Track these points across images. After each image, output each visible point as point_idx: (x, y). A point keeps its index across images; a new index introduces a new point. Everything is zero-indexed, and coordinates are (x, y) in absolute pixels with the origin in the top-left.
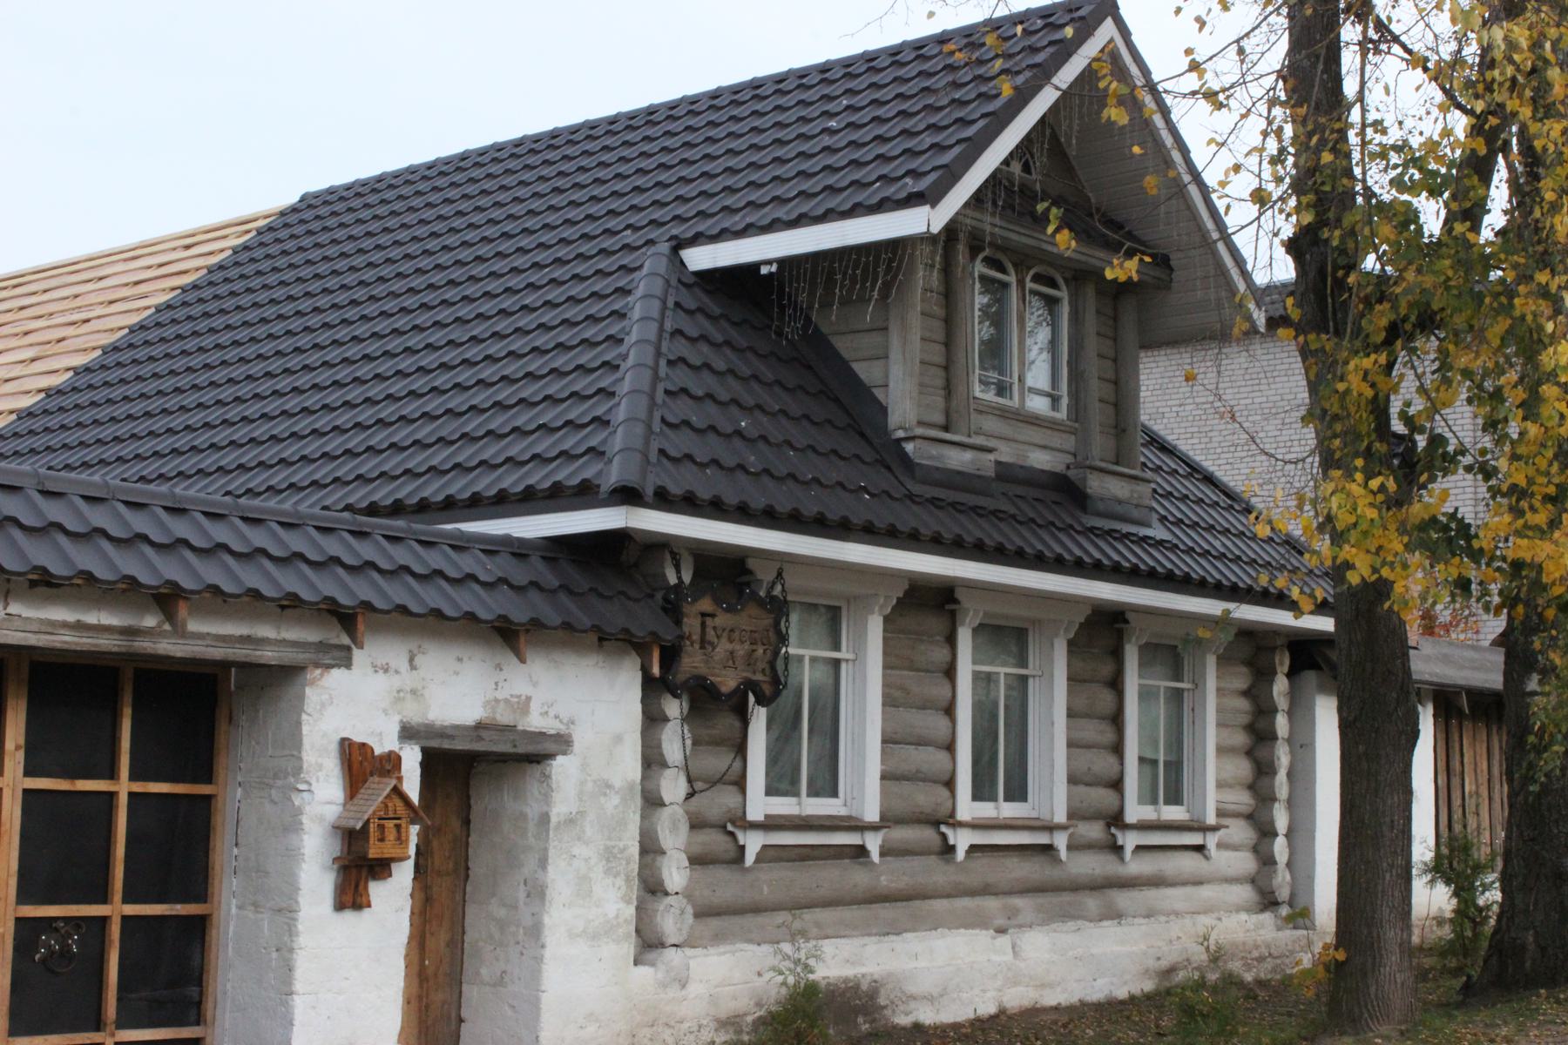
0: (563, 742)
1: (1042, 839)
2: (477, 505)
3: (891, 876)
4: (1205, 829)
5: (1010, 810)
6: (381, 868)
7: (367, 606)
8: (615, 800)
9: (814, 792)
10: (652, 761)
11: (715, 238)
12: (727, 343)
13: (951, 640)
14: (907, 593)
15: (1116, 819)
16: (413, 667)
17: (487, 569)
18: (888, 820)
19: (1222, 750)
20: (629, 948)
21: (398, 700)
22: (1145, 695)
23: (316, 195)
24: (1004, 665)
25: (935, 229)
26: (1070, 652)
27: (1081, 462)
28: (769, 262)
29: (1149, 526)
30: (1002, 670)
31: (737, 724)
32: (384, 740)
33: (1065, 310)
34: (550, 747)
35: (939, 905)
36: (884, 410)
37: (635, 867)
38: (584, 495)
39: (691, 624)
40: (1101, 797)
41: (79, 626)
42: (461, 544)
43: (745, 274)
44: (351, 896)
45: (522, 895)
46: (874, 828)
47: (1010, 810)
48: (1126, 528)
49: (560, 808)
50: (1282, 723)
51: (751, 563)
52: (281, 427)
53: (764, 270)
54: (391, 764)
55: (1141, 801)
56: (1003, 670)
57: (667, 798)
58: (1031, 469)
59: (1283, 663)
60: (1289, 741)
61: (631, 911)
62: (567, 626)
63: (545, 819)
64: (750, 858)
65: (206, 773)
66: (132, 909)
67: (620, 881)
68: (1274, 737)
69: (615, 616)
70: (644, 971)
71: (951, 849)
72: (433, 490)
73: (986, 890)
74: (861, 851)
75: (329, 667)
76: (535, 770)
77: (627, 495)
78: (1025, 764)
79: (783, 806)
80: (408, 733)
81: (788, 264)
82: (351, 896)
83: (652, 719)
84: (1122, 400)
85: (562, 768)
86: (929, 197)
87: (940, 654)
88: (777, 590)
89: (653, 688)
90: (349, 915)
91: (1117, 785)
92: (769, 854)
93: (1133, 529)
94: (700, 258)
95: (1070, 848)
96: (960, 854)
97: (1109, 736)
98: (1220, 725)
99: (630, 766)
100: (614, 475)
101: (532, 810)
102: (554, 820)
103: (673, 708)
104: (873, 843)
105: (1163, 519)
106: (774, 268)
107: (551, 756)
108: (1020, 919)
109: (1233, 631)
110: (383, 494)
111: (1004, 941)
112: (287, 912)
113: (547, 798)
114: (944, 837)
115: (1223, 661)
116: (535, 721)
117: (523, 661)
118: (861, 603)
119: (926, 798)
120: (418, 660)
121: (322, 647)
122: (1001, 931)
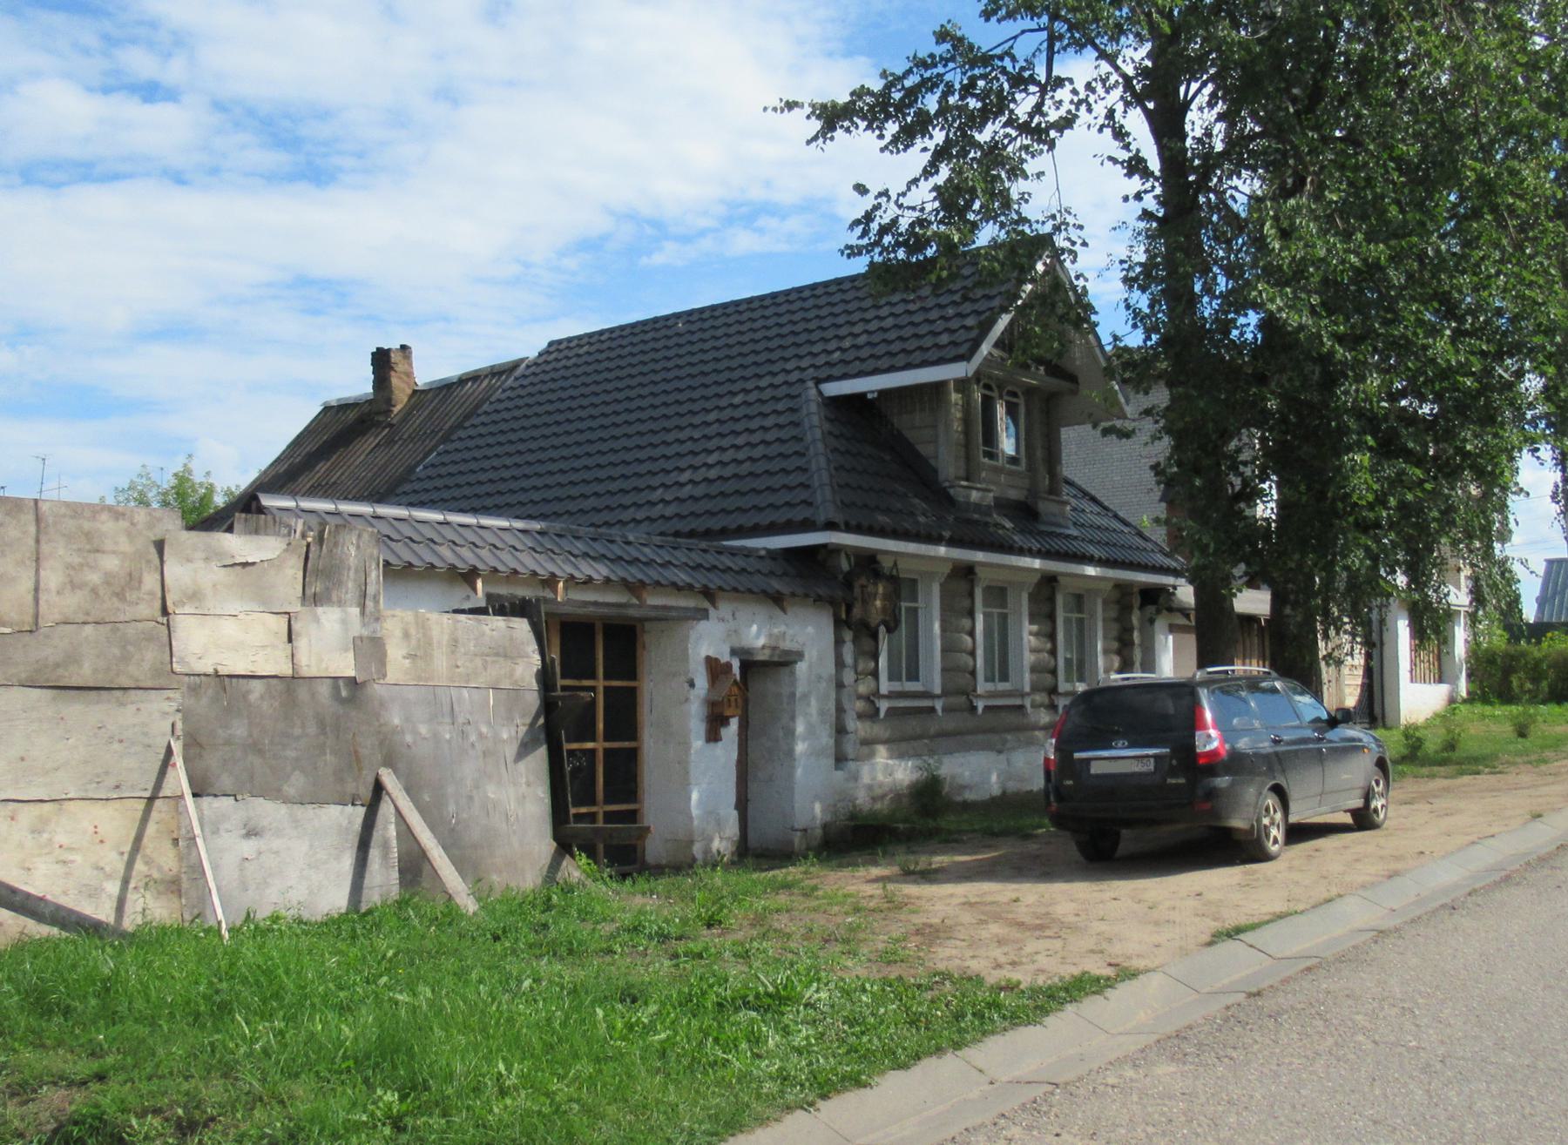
0: (800, 655)
1: (1018, 702)
2: (741, 532)
3: (951, 724)
4: (1023, 695)
5: (1002, 686)
6: (725, 721)
7: (720, 588)
8: (824, 684)
9: (909, 679)
10: (840, 664)
11: (845, 376)
12: (842, 435)
13: (971, 595)
14: (952, 571)
15: (1053, 691)
16: (734, 618)
17: (740, 562)
18: (945, 693)
19: (1106, 652)
20: (831, 761)
21: (729, 636)
22: (1067, 621)
23: (560, 342)
24: (995, 607)
25: (970, 375)
26: (1030, 601)
27: (1033, 492)
28: (873, 392)
29: (1068, 528)
30: (995, 610)
31: (873, 643)
32: (725, 657)
33: (1022, 410)
34: (791, 658)
35: (969, 738)
36: (935, 471)
37: (834, 719)
38: (807, 526)
39: (857, 591)
40: (1048, 678)
41: (596, 604)
42: (733, 552)
43: (860, 398)
44: (713, 736)
45: (781, 734)
46: (938, 697)
47: (1002, 686)
48: (1059, 530)
49: (800, 689)
50: (1136, 635)
51: (879, 557)
52: (474, 466)
53: (870, 396)
54: (729, 666)
55: (987, 680)
56: (996, 611)
57: (846, 683)
58: (1008, 500)
59: (1137, 601)
60: (1140, 645)
61: (832, 742)
62: (735, 590)
63: (793, 695)
64: (882, 714)
65: (632, 674)
66: (608, 745)
67: (827, 726)
68: (1132, 643)
69: (822, 591)
70: (839, 773)
71: (974, 708)
72: (715, 524)
73: (992, 730)
74: (932, 710)
75: (699, 620)
76: (785, 671)
77: (831, 526)
78: (917, 656)
79: (897, 686)
80: (734, 652)
81: (884, 394)
82: (713, 736)
83: (839, 642)
84: (1052, 457)
85: (801, 668)
86: (966, 357)
87: (966, 603)
88: (894, 572)
89: (839, 624)
90: (712, 745)
91: (1054, 672)
92: (892, 712)
93: (1062, 531)
94: (833, 389)
95: (944, 710)
96: (980, 710)
97: (1049, 646)
98: (1105, 637)
99: (830, 668)
100: (822, 518)
101: (785, 691)
102: (798, 695)
103: (848, 635)
104: (938, 705)
105: (1075, 524)
106: (876, 395)
107: (795, 662)
108: (1008, 745)
109: (1112, 584)
110: (684, 526)
111: (1002, 757)
112: (686, 746)
113: (793, 683)
114: (971, 702)
115: (1105, 603)
116: (787, 645)
117: (784, 610)
118: (930, 575)
119: (963, 680)
120: (737, 614)
121: (697, 610)
122: (1000, 752)
